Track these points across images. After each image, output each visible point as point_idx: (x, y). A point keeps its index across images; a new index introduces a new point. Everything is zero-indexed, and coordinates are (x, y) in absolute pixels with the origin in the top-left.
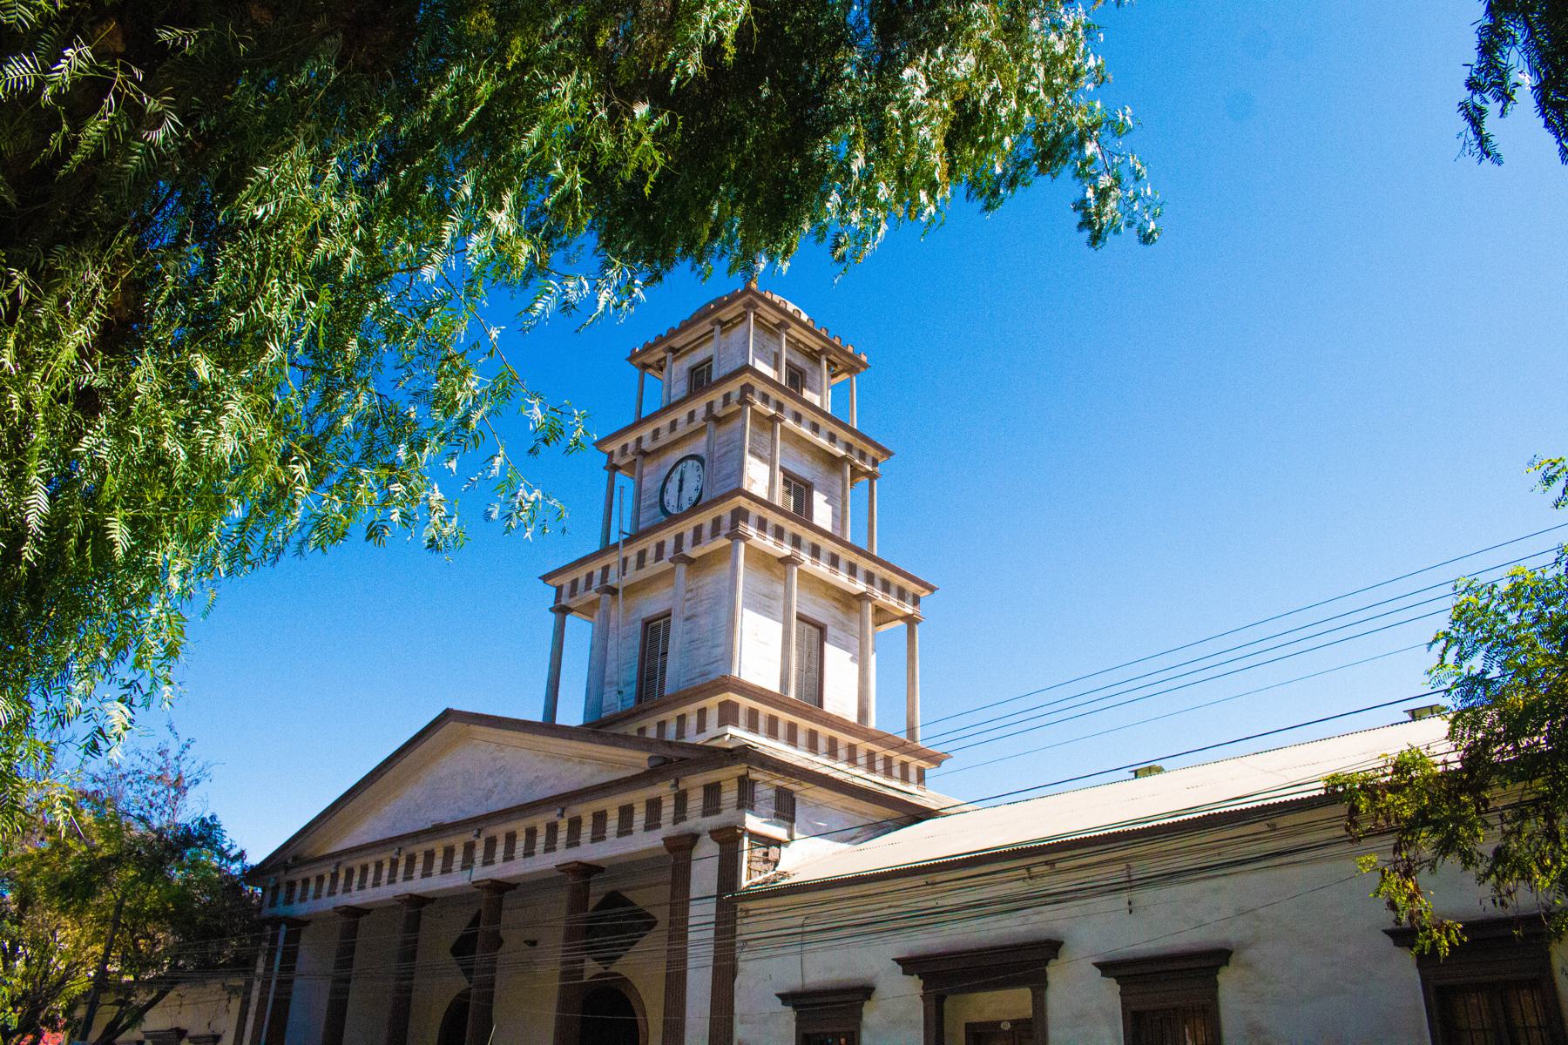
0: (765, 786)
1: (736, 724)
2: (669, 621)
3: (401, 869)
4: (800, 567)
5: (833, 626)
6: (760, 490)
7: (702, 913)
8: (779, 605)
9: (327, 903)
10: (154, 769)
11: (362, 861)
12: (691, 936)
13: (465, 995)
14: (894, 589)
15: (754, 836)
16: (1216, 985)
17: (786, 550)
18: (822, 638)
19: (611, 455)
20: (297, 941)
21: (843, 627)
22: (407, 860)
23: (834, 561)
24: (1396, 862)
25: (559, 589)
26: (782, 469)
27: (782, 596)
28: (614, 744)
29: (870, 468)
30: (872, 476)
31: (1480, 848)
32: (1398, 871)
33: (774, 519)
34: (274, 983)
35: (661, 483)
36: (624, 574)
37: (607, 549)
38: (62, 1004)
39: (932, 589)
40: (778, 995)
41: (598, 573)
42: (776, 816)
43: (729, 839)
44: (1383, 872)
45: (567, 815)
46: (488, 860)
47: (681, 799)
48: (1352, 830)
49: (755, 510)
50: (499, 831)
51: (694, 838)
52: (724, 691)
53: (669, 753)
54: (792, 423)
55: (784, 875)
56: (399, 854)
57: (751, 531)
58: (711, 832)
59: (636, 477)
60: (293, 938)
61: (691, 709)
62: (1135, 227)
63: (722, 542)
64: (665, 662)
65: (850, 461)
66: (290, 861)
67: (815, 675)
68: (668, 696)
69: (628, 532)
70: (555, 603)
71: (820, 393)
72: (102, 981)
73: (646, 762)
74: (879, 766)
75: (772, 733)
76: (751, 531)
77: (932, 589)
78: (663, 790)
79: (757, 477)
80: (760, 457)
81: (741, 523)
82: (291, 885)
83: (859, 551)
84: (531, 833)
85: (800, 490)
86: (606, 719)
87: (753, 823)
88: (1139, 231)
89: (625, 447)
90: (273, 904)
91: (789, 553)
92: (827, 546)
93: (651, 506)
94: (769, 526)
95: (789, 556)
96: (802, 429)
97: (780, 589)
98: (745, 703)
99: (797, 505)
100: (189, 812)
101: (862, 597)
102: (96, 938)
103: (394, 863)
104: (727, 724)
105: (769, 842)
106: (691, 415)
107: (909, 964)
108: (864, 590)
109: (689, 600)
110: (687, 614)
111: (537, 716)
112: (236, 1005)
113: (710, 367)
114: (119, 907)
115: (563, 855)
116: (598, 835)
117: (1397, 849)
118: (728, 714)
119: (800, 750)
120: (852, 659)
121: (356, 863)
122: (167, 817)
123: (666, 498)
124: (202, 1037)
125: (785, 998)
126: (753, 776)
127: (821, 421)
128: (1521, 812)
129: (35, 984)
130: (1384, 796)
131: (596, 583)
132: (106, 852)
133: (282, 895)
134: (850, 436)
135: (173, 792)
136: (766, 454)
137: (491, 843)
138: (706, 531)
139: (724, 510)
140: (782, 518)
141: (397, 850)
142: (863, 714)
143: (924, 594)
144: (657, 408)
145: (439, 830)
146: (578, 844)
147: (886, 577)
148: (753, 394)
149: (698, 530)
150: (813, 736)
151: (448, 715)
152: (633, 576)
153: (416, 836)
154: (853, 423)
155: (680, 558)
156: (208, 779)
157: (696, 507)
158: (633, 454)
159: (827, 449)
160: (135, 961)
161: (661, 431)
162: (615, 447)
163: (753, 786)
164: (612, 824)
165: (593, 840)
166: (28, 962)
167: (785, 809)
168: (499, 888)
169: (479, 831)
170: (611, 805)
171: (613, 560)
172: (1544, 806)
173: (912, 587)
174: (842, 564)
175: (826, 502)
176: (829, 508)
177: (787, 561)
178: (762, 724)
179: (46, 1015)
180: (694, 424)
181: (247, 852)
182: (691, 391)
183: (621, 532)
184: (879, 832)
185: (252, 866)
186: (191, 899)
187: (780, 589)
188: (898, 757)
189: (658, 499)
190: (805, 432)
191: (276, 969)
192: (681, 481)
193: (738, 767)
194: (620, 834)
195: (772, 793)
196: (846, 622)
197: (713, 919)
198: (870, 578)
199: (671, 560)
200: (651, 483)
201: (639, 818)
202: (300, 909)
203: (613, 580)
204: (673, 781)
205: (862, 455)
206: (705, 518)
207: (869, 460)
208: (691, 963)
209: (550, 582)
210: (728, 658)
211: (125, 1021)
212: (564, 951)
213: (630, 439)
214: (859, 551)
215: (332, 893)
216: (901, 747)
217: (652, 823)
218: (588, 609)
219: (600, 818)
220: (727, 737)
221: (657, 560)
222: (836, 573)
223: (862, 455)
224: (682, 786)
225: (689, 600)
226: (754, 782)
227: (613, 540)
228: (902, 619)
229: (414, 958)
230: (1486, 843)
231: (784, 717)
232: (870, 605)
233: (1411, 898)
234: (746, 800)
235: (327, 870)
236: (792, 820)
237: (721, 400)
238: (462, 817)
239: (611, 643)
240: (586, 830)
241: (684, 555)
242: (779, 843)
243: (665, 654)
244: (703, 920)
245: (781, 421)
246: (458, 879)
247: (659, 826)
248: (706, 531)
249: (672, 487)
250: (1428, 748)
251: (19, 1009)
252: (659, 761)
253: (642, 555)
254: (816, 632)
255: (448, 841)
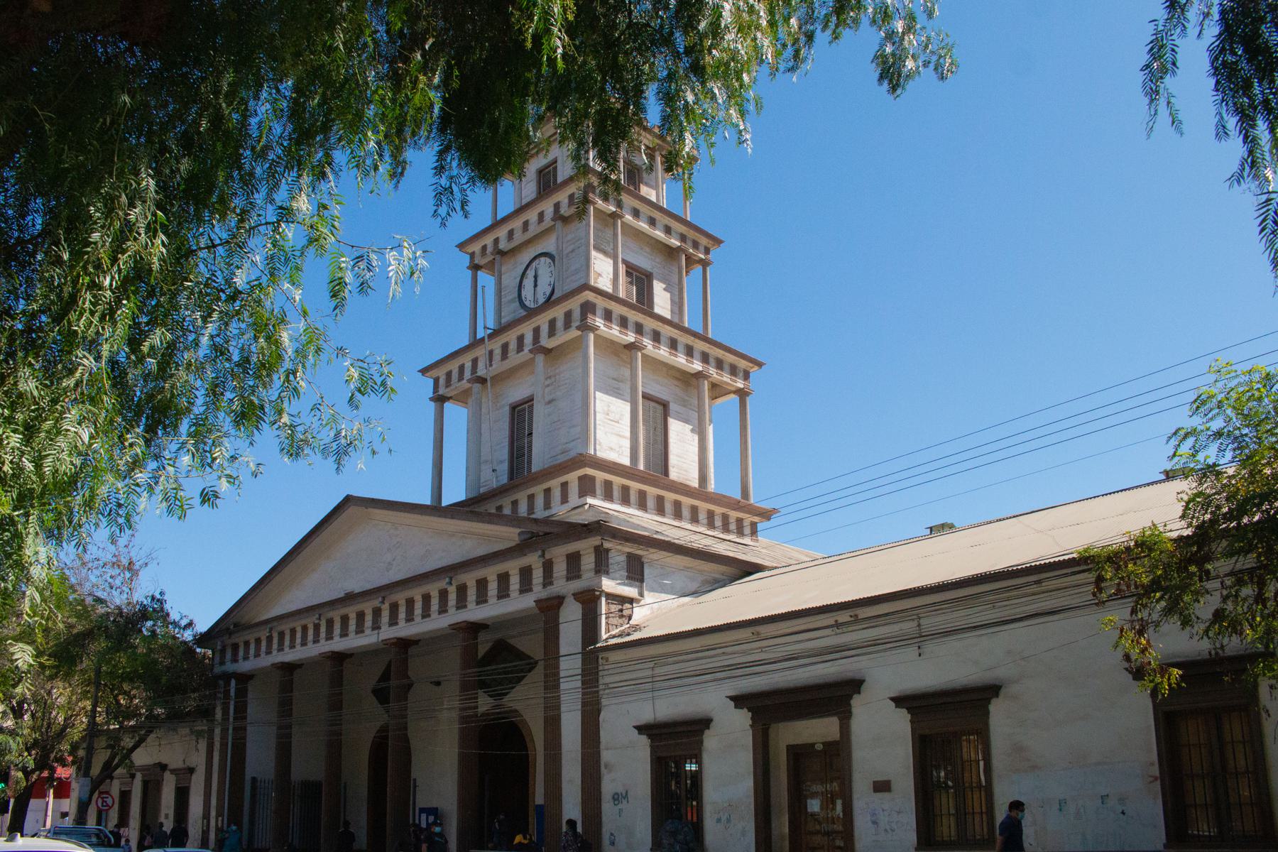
0: (618, 553)
1: (593, 494)
2: (533, 405)
3: (323, 629)
4: (643, 351)
5: (675, 403)
6: (605, 284)
7: (570, 666)
8: (626, 388)
9: (266, 661)
10: (109, 556)
11: (291, 625)
12: (563, 686)
13: (383, 731)
14: (726, 367)
15: (612, 597)
16: (987, 713)
17: (631, 337)
18: (666, 414)
19: (472, 255)
20: (246, 696)
21: (684, 403)
22: (327, 623)
23: (673, 344)
24: (1132, 622)
25: (436, 381)
26: (624, 261)
27: (629, 379)
28: (489, 522)
29: (703, 257)
30: (705, 264)
31: (1198, 613)
32: (1134, 628)
33: (618, 310)
34: (230, 731)
35: (519, 279)
36: (491, 365)
37: (476, 343)
38: (65, 747)
39: (760, 365)
40: (635, 727)
41: (468, 365)
42: (628, 578)
43: (590, 600)
44: (1122, 630)
45: (455, 583)
46: (393, 622)
47: (548, 567)
48: (1098, 595)
49: (601, 303)
50: (400, 597)
51: (559, 600)
52: (580, 468)
53: (535, 529)
54: (630, 218)
55: (636, 628)
56: (320, 619)
57: (599, 322)
58: (573, 595)
59: (496, 274)
60: (242, 693)
61: (555, 484)
62: (932, 66)
63: (574, 333)
64: (530, 443)
65: (684, 251)
66: (232, 627)
67: (660, 447)
68: (535, 473)
69: (492, 327)
70: (534, 345)
71: (656, 187)
72: (93, 731)
73: (517, 536)
74: (718, 523)
75: (625, 501)
76: (599, 322)
77: (760, 365)
78: (533, 560)
79: (603, 271)
80: (605, 253)
81: (589, 316)
82: (235, 647)
83: (695, 335)
84: (427, 598)
85: (641, 280)
86: (484, 494)
87: (608, 585)
88: (936, 69)
89: (484, 248)
90: (222, 663)
91: (632, 340)
92: (667, 331)
93: (511, 301)
94: (614, 316)
95: (632, 343)
96: (640, 223)
97: (627, 373)
98: (600, 476)
99: (640, 294)
100: (142, 592)
101: (699, 375)
102: (84, 695)
103: (317, 627)
104: (586, 495)
105: (623, 600)
106: (541, 215)
107: (739, 700)
108: (701, 369)
109: (548, 386)
110: (547, 399)
111: (426, 500)
112: (203, 745)
113: (555, 168)
114: (98, 672)
115: (455, 616)
116: (482, 599)
117: (1134, 612)
118: (587, 486)
119: (650, 513)
120: (692, 431)
121: (286, 627)
122: (125, 596)
123: (523, 293)
124: (180, 770)
125: (641, 729)
126: (607, 545)
127: (657, 215)
128: (1239, 578)
129: (42, 734)
130: (1126, 567)
131: (467, 374)
132: (79, 628)
133: (229, 655)
134: (685, 228)
135: (128, 575)
136: (609, 249)
137: (394, 608)
138: (560, 324)
139: (574, 304)
140: (625, 309)
141: (317, 616)
142: (703, 478)
143: (754, 370)
144: (511, 209)
145: (350, 598)
146: (465, 607)
147: (720, 356)
148: (594, 314)
149: (552, 323)
150: (660, 500)
151: (348, 500)
152: (498, 366)
153: (332, 604)
154: (686, 216)
155: (538, 349)
156: (155, 562)
157: (550, 302)
158: (492, 254)
159: (664, 241)
160: (117, 713)
161: (515, 232)
162: (476, 247)
163: (607, 554)
164: (493, 587)
165: (478, 603)
166: (33, 716)
167: (635, 573)
168: (404, 645)
169: (384, 598)
170: (491, 573)
171: (480, 352)
172: (1257, 576)
173: (743, 364)
174: (680, 347)
175: (665, 289)
176: (668, 295)
177: (631, 347)
178: (616, 493)
179: (55, 756)
180: (544, 224)
181: (195, 622)
182: (540, 193)
183: (485, 328)
184: (716, 585)
185: (201, 634)
186: (155, 662)
187: (627, 373)
188: (734, 515)
189: (516, 295)
190: (643, 226)
191: (231, 719)
192: (536, 277)
193: (594, 539)
194: (500, 597)
195: (623, 558)
196: (687, 398)
197: (579, 671)
198: (705, 358)
199: (531, 351)
200: (510, 279)
201: (515, 582)
202: (244, 666)
203: (481, 372)
204: (540, 553)
205: (696, 245)
206: (558, 312)
207: (702, 249)
208: (563, 709)
209: (428, 374)
210: (585, 434)
211: (116, 760)
212: (461, 700)
213: (488, 240)
214: (695, 335)
215: (269, 652)
216: (736, 506)
217: (526, 587)
218: (462, 398)
219: (482, 584)
220: (587, 507)
221: (518, 352)
222: (676, 356)
223: (696, 245)
224: (547, 556)
225: (548, 386)
226: (608, 551)
227: (480, 334)
228: (735, 392)
229: (341, 708)
230: (1205, 608)
231: (635, 486)
232: (706, 382)
233: (1143, 651)
234: (602, 567)
235: (263, 634)
236: (642, 580)
237: (566, 201)
238: (368, 587)
239: (485, 427)
240: (472, 594)
241: (541, 346)
242: (631, 601)
243: (530, 434)
244: (571, 672)
245: (621, 217)
246: (368, 639)
247: (531, 590)
248: (560, 324)
249: (528, 282)
250: (1165, 526)
251: (33, 752)
252: (527, 536)
253: (505, 347)
254: (660, 408)
255: (359, 607)
